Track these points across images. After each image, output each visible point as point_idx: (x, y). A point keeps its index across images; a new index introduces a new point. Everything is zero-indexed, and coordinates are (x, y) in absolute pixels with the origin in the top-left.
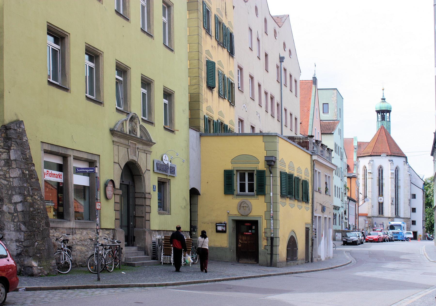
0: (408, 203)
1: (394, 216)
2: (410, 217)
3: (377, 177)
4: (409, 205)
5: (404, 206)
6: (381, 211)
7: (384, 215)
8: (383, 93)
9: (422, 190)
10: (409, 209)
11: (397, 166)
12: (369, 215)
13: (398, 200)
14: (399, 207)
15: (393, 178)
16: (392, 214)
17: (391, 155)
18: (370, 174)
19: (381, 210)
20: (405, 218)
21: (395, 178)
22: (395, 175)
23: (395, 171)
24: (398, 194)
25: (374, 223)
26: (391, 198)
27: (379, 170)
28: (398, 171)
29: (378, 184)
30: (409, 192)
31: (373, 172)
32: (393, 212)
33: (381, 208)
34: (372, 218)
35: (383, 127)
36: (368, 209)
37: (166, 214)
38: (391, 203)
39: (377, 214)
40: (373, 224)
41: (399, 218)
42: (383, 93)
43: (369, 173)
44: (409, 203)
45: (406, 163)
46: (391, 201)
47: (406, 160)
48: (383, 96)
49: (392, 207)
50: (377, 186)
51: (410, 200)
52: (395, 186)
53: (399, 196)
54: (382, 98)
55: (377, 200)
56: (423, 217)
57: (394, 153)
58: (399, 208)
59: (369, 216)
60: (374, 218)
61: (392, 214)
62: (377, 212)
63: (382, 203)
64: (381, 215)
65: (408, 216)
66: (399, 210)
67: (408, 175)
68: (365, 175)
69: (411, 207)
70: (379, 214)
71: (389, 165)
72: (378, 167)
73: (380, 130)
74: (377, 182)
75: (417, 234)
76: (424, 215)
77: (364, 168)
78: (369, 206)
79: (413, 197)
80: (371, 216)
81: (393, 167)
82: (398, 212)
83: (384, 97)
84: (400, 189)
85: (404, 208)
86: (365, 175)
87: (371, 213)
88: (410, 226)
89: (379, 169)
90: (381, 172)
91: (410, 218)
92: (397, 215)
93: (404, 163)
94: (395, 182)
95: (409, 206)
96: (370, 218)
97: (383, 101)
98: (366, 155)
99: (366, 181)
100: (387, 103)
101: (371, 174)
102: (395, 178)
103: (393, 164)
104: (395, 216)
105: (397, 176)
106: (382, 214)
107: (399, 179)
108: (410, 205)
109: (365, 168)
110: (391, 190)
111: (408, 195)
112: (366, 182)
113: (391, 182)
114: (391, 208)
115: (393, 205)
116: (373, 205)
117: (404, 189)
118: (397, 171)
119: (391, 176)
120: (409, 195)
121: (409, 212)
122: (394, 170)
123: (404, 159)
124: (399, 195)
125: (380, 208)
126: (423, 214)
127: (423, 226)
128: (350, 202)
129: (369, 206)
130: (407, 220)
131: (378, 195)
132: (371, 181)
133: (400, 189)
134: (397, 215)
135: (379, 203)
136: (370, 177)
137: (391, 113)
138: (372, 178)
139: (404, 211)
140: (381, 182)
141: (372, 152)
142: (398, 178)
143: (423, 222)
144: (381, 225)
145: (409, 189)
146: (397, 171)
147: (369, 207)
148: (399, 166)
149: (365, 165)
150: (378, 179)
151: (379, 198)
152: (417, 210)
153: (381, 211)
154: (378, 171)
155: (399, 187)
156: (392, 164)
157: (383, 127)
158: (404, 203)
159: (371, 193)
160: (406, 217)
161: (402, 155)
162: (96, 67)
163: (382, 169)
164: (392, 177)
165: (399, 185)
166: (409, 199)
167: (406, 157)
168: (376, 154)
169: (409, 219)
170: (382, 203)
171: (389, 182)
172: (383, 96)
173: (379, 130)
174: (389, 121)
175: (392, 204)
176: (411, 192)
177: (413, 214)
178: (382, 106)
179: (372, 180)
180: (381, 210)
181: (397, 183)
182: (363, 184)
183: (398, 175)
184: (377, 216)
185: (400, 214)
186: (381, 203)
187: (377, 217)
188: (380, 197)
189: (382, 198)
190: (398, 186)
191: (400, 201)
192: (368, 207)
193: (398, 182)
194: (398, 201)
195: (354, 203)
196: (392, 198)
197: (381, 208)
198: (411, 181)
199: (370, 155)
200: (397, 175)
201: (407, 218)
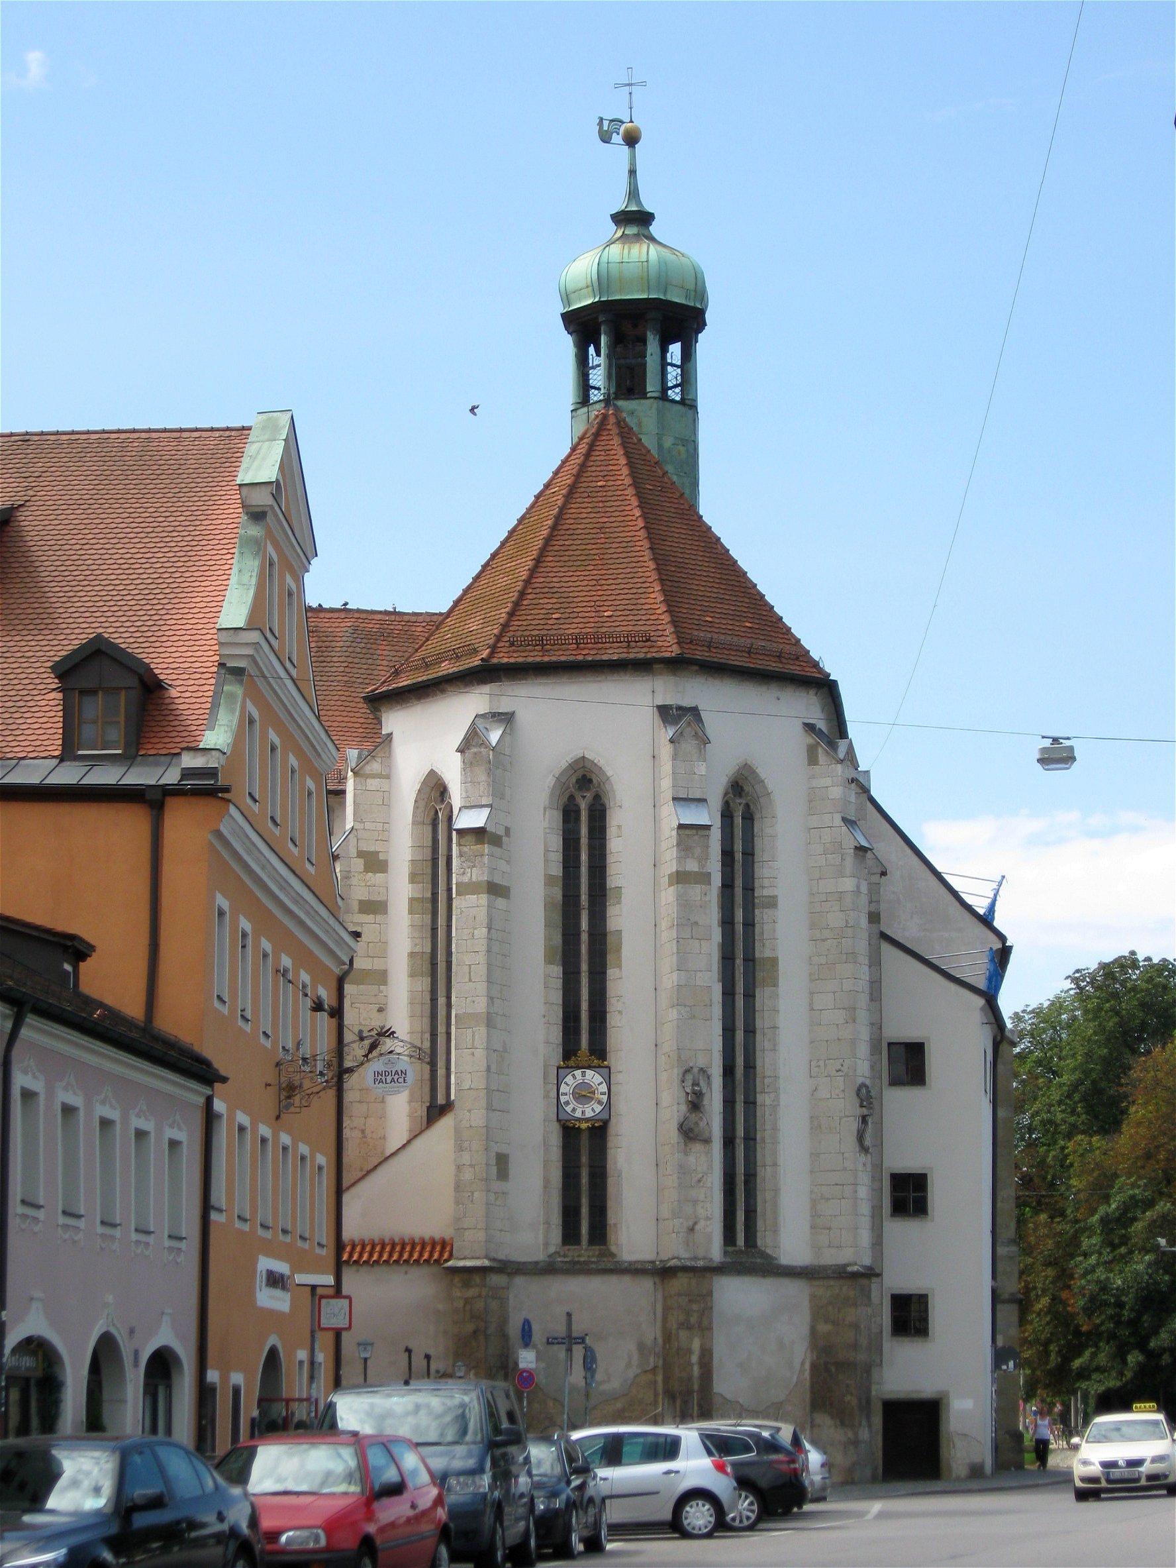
0: (853, 1125)
1: (715, 1251)
2: (867, 1261)
3: (549, 880)
4: (860, 1137)
5: (815, 1155)
6: (585, 1210)
7: (613, 1249)
8: (632, 172)
9: (980, 1002)
10: (865, 1179)
11: (746, 766)
12: (467, 1253)
13: (759, 1098)
14: (769, 1161)
15: (704, 878)
16: (692, 1229)
17: (676, 665)
18: (472, 848)
19: (585, 1201)
20: (824, 1268)
21: (727, 886)
22: (727, 855)
23: (727, 815)
24: (759, 1037)
25: (514, 1328)
26: (676, 1072)
27: (569, 814)
28: (749, 818)
29: (558, 939)
30: (863, 1016)
31: (507, 830)
32: (701, 1212)
33: (585, 1180)
34: (496, 1279)
35: (612, 420)
36: (458, 1187)
37: (725, 1398)
38: (681, 1127)
39: (546, 1244)
40: (505, 1337)
41: (769, 1268)
42: (632, 172)
43: (470, 838)
44: (864, 1119)
45: (832, 745)
46: (684, 1108)
47: (828, 720)
48: (633, 193)
49: (692, 1159)
50: (549, 960)
51: (866, 1098)
52: (727, 958)
53: (764, 1061)
54: (619, 204)
55: (546, 1096)
56: (1000, 1269)
57: (709, 645)
58: (760, 1172)
59: (461, 1264)
60: (519, 1281)
61: (692, 1229)
62: (547, 1223)
63: (592, 1129)
64: (584, 1251)
65: (856, 1253)
66: (769, 1195)
67: (850, 861)
68: (435, 861)
69: (878, 1166)
70: (570, 1234)
71: (666, 751)
72: (561, 783)
73: (583, 449)
74: (547, 925)
75: (943, 1428)
76: (1001, 1251)
77: (429, 799)
78: (466, 1158)
79: (901, 1069)
80: (486, 1263)
81: (702, 769)
82: (751, 1213)
83: (639, 203)
84: (768, 990)
85: (812, 1172)
86: (435, 861)
87: (481, 1236)
88: (876, 1348)
89: (571, 798)
90: (591, 830)
91: (871, 1273)
92: (741, 1240)
93: (810, 740)
94: (727, 922)
95: (864, 1149)
96: (477, 1279)
97: (631, 230)
98: (447, 668)
99: (441, 921)
100: (660, 248)
101: (486, 848)
102: (717, 880)
103: (704, 741)
104: (726, 1253)
105: (738, 867)
106: (600, 1233)
107: (766, 892)
108: (868, 1142)
109: (437, 794)
110: (684, 996)
111: (853, 1042)
112: (449, 927)
113: (686, 922)
114: (683, 1170)
115: (697, 1147)
116: (504, 1149)
117: (812, 993)
118: (738, 821)
119: (680, 859)
120: (863, 1049)
121: (865, 1209)
122: (716, 803)
123: (805, 706)
124: (767, 1045)
125: (577, 1176)
126: (994, 1232)
127: (1000, 1343)
128: (24, 1032)
129: (466, 1158)
130: (847, 1290)
131: (556, 1058)
132: (484, 911)
133: (776, 985)
134: (741, 1240)
135: (569, 1132)
136: (477, 875)
137: (705, 343)
138: (495, 890)
139: (814, 1203)
140: (584, 925)
141: (499, 638)
142: (749, 889)
143: (999, 1315)
144: (569, 1350)
145: (863, 984)
146: (738, 821)
147: (468, 1175)
148: (762, 773)
149: (432, 773)
150: (558, 893)
151: (569, 1079)
152: (937, 1195)
153: (585, 1210)
154: (557, 816)
155: (759, 975)
156: (689, 746)
157: (612, 420)
158: (816, 1126)
159: (482, 1030)
160: (831, 1258)
161: (793, 668)
162: (74, 971)
163: (597, 797)
164: (692, 866)
165: (768, 954)
166: (863, 1085)
167: (827, 689)
168: (535, 657)
169: (855, 1276)
170: (600, 1131)
171: (664, 925)
172: (633, 193)
173: (573, 449)
174: (682, 402)
175: (689, 1133)
176: (877, 1026)
177: (900, 1230)
178: (614, 269)
179: (490, 906)
180: (585, 1201)
181: (739, 928)
182: (412, 955)
183: (749, 854)
184: (540, 1256)
185: (776, 1231)
186: (584, 1126)
187: (548, 1269)
188: (578, 1073)
189: (593, 1077)
190: (750, 960)
191: (775, 1107)
192: (459, 1168)
193: (749, 924)
194: (751, 1103)
195: (192, 1093)
196: (688, 1071)
197: (585, 1180)
198: (874, 918)
199: (476, 662)
200: (739, 856)
201: (842, 1274)
